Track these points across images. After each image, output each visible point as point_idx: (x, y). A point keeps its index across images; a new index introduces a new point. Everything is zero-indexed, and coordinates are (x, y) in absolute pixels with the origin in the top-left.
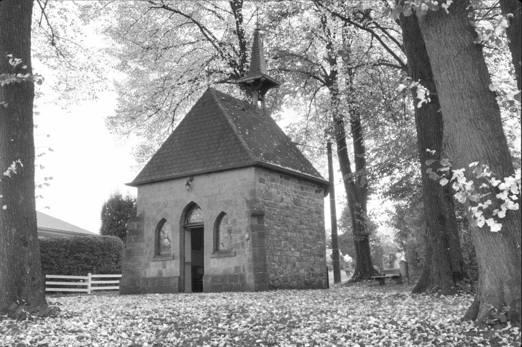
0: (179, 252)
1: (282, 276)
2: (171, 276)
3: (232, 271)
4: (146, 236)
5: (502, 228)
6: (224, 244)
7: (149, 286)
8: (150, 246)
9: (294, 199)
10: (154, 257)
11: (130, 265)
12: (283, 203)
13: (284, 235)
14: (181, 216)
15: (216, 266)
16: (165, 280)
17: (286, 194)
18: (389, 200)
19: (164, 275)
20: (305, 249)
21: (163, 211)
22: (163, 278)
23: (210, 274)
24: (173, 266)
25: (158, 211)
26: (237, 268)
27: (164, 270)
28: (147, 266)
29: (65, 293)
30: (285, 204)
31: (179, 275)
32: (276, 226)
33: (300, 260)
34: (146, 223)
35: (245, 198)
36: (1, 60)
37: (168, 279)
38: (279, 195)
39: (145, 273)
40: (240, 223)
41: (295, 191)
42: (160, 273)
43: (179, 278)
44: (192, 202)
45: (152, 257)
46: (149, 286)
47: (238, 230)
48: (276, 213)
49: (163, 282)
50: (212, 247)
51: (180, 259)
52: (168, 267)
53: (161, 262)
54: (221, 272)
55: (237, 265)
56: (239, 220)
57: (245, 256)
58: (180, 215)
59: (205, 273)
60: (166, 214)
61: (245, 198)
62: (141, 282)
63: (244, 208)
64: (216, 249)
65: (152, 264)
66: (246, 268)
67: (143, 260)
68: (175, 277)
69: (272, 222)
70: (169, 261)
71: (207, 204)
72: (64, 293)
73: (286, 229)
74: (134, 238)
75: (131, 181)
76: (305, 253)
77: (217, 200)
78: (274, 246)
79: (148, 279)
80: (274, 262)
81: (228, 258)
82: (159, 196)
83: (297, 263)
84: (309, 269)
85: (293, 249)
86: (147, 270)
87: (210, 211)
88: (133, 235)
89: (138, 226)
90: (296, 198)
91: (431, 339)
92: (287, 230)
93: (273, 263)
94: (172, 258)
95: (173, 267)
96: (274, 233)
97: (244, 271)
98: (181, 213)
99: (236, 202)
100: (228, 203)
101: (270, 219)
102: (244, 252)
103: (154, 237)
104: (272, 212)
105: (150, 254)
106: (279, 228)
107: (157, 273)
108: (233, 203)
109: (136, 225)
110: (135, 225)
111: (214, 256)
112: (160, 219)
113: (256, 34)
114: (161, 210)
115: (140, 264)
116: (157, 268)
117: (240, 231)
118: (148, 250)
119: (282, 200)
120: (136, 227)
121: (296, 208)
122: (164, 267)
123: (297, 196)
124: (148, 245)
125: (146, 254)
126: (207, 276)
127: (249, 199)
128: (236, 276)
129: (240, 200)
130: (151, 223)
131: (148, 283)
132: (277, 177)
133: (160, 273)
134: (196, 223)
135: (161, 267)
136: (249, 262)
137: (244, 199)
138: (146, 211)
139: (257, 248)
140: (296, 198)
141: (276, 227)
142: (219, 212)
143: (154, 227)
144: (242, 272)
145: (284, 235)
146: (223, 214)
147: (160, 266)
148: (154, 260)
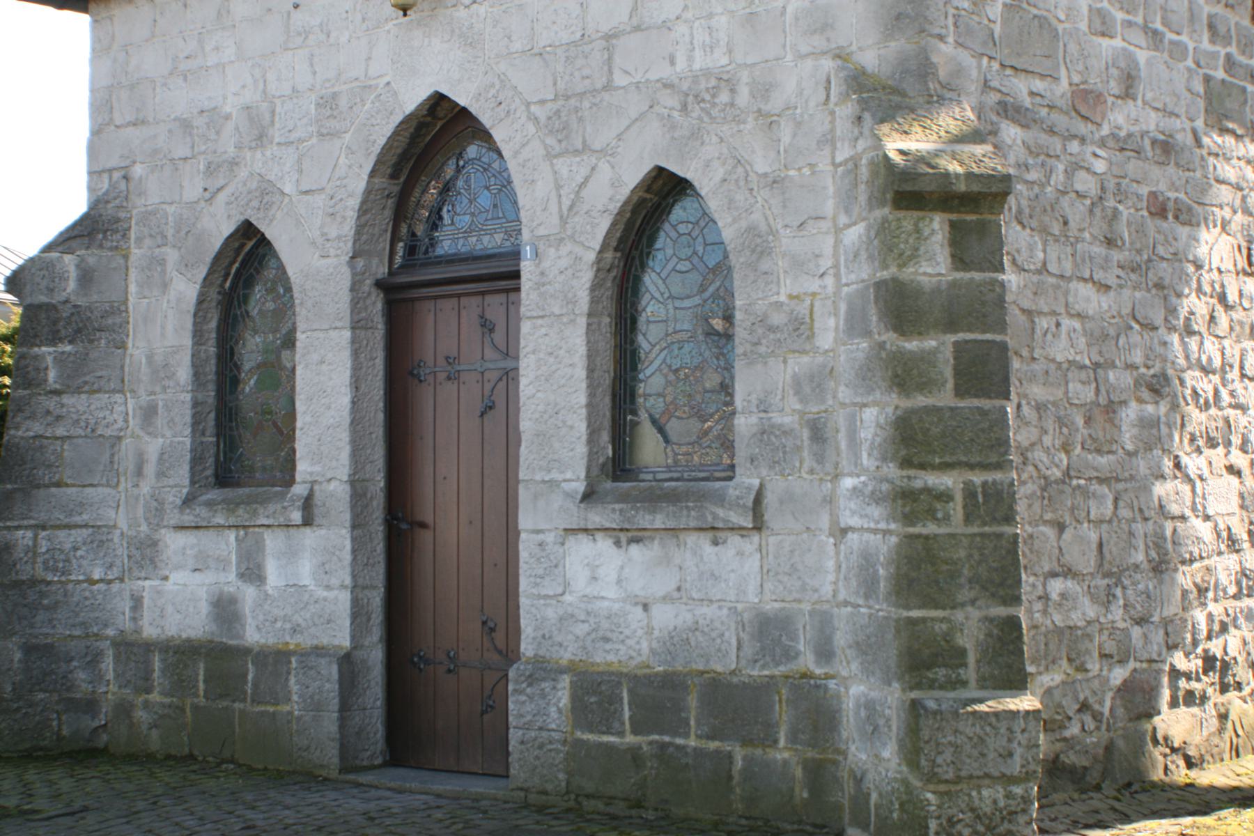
0: (344, 472)
2: (293, 642)
3: (727, 656)
4: (137, 349)
5: (936, 291)
6: (673, 427)
8: (160, 421)
9: (1207, 79)
10: (188, 501)
11: (33, 550)
12: (1132, 108)
13: (1138, 357)
14: (363, 210)
17: (1155, 37)
19: (253, 635)
21: (243, 173)
22: (246, 651)
23: (566, 656)
24: (305, 572)
25: (211, 170)
26: (770, 631)
27: (249, 593)
28: (146, 554)
30: (1152, 122)
31: (343, 640)
32: (1086, 290)
34: (136, 253)
35: (841, 56)
37: (275, 660)
38: (1107, 45)
39: (137, 603)
41: (1211, 27)
42: (225, 609)
43: (348, 663)
44: (438, 101)
45: (174, 497)
46: (155, 697)
47: (777, 319)
48: (1085, 183)
50: (581, 449)
51: (357, 524)
53: (232, 536)
57: (842, 532)
58: (354, 202)
59: (527, 648)
60: (267, 191)
61: (841, 56)
62: (108, 665)
63: (829, 140)
64: (616, 464)
65: (175, 543)
66: (841, 639)
67: (120, 509)
68: (319, 651)
69: (1054, 251)
70: (280, 534)
74: (60, 360)
77: (620, 80)
78: (1066, 448)
79: (149, 647)
80: (1068, 572)
81: (702, 542)
82: (221, 67)
87: (562, 165)
88: (54, 339)
89: (86, 277)
90: (1220, 74)
93: (1056, 586)
94: (297, 516)
95: (306, 580)
96: (1067, 344)
97: (825, 652)
98: (359, 184)
99: (764, 90)
100: (702, 97)
101: (1044, 231)
102: (830, 501)
103: (186, 359)
104: (1059, 177)
105: (161, 474)
107: (205, 608)
108: (743, 97)
109: (73, 273)
111: (596, 518)
112: (227, 229)
114: (234, 163)
115: (99, 536)
116: (209, 577)
117: (802, 328)
118: (153, 448)
119: (1129, 85)
120: (72, 285)
122: (252, 573)
123: (1230, 63)
124: (149, 413)
125: (139, 472)
126: (544, 670)
127: (870, 59)
128: (761, 691)
130: (172, 256)
131: (147, 676)
133: (225, 609)
135: (232, 576)
136: (869, 587)
137: (828, 64)
138: (138, 170)
140: (1220, 74)
141: (1086, 297)
142: (633, 175)
143: (185, 288)
145: (1138, 357)
146: (664, 191)
147: (223, 564)
148: (188, 519)
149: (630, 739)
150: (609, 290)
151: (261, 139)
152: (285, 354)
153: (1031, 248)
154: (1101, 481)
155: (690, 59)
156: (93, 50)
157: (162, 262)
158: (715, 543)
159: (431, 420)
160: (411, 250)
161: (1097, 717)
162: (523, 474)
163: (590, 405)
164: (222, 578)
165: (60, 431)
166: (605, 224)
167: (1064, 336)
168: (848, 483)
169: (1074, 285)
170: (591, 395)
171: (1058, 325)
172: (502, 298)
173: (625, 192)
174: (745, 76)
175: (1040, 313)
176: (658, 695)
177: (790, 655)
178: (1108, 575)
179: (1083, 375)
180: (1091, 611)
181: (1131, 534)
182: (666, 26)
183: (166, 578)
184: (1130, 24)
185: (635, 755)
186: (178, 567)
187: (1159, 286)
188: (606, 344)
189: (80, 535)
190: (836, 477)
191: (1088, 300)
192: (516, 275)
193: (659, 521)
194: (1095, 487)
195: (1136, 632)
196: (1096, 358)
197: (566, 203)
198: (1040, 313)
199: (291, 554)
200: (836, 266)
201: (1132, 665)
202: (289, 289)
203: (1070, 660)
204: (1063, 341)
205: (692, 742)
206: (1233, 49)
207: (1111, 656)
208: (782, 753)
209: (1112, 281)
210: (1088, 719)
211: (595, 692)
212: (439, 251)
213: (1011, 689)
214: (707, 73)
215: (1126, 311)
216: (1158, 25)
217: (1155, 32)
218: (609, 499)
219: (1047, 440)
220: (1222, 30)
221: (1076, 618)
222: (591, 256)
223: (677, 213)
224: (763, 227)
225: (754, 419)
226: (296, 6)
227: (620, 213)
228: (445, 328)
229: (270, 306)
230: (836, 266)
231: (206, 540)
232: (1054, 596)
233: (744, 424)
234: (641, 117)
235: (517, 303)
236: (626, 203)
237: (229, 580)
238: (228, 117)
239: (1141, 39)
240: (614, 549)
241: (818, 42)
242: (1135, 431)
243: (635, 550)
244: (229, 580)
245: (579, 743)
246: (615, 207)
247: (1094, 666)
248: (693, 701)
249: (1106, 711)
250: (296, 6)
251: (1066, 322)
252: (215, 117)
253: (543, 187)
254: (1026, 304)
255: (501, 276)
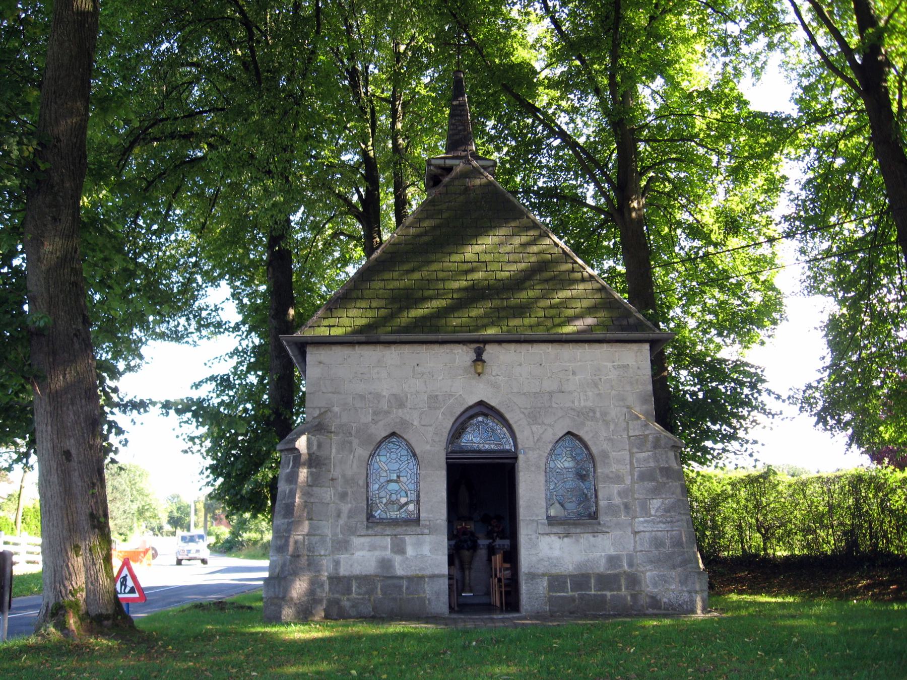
7: (354, 595)
15: (556, 553)
16: (405, 583)
24: (426, 550)
25: (375, 413)
26: (613, 560)
27: (397, 559)
36: (894, 45)
37: (416, 580)
40: (618, 461)
46: (354, 595)
47: (611, 475)
49: (401, 587)
52: (410, 551)
54: (571, 568)
55: (612, 552)
56: (613, 454)
71: (526, 412)
79: (349, 579)
86: (343, 557)
87: (534, 428)
91: (348, 600)
100: (587, 414)
108: (598, 415)
116: (377, 553)
122: (400, 549)
126: (533, 576)
129: (615, 412)
130: (355, 442)
132: (512, 347)
133: (385, 564)
134: (480, 451)
144: (626, 568)
149: (570, 593)
151: (401, 405)
155: (580, 403)
164: (383, 553)
165: (312, 500)
174: (598, 410)
176: (580, 580)
177: (621, 566)
182: (570, 392)
185: (573, 599)
189: (317, 538)
193: (578, 531)
197: (536, 439)
199: (419, 544)
205: (593, 592)
208: (623, 591)
211: (556, 581)
213: (366, 576)
214: (585, 407)
218: (245, 551)
225: (606, 502)
231: (378, 540)
233: (602, 503)
234: (562, 417)
237: (388, 553)
238: (385, 396)
240: (558, 540)
241: (621, 403)
243: (565, 539)
245: (551, 597)
248: (593, 581)
252: (378, 396)
253: (527, 432)
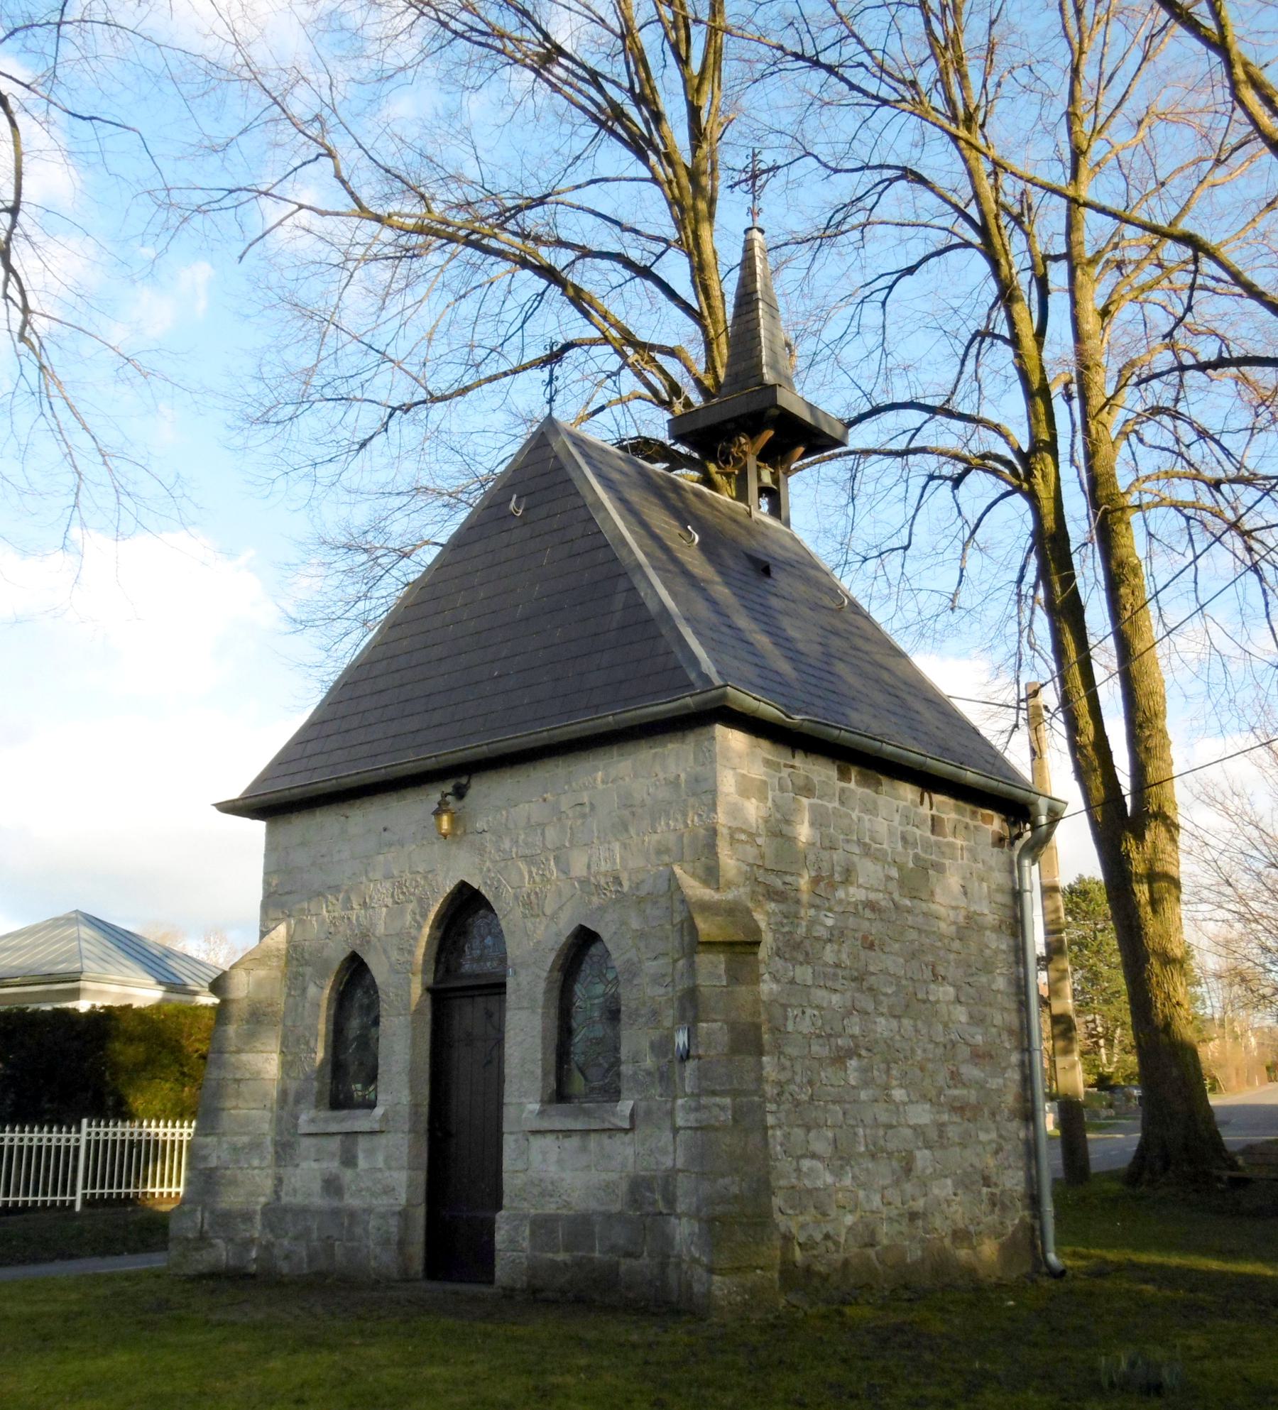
1: (849, 1219)
18: (1231, 383)
20: (956, 1092)
29: (1067, 613)
33: (936, 1139)
43: (404, 1215)
44: (463, 887)
69: (799, 969)
72: (1067, 613)
73: (867, 1003)
75: (235, 792)
76: (959, 1108)
80: (814, 1156)
83: (918, 1154)
84: (977, 1177)
85: (898, 1094)
92: (871, 1008)
93: (806, 1164)
102: (671, 1113)
106: (835, 998)
110: (113, 1023)
113: (747, 264)
121: (909, 911)
133: (332, 1186)
139: (727, 1101)
150: (556, 993)
152: (373, 1030)
153: (786, 970)
154: (834, 1102)
156: (267, 849)
157: (303, 975)
158: (610, 1137)
159: (857, 737)
160: (448, 971)
161: (837, 1244)
162: (506, 1100)
163: (544, 1059)
166: (551, 957)
167: (807, 1019)
168: (680, 1102)
169: (813, 990)
170: (544, 1054)
171: (803, 1013)
172: (497, 997)
173: (563, 939)
175: (790, 1006)
176: (580, 1227)
178: (841, 1158)
179: (821, 1041)
180: (829, 1179)
181: (855, 1134)
183: (297, 1166)
184: (848, 841)
186: (306, 1158)
187: (871, 989)
188: (553, 1023)
190: (675, 1098)
191: (823, 998)
192: (503, 985)
194: (831, 1106)
195: (861, 1194)
196: (829, 1031)
198: (790, 1006)
200: (673, 981)
201: (858, 1214)
202: (377, 992)
203: (815, 1207)
204: (808, 1021)
206: (919, 851)
207: (844, 1207)
209: (838, 987)
210: (830, 1244)
212: (463, 970)
215: (849, 1004)
216: (867, 840)
217: (865, 844)
219: (798, 1079)
220: (910, 839)
221: (820, 1184)
222: (545, 975)
223: (593, 950)
224: (636, 959)
226: (385, 830)
227: (561, 950)
228: (468, 1015)
229: (366, 1001)
230: (673, 981)
232: (805, 1169)
235: (504, 1001)
236: (564, 944)
239: (856, 850)
242: (856, 1074)
244: (334, 1166)
246: (557, 947)
247: (833, 1212)
249: (842, 1241)
250: (385, 830)
251: (809, 1011)
253: (477, 421)
254: (783, 1001)
255: (497, 988)
